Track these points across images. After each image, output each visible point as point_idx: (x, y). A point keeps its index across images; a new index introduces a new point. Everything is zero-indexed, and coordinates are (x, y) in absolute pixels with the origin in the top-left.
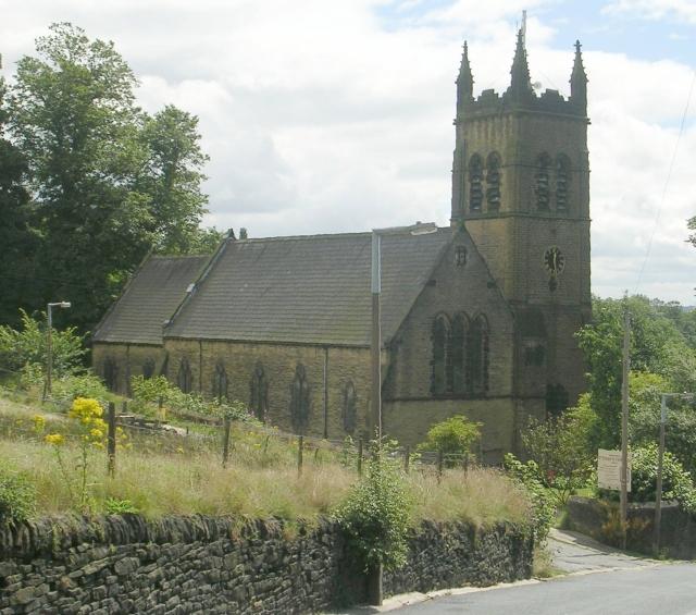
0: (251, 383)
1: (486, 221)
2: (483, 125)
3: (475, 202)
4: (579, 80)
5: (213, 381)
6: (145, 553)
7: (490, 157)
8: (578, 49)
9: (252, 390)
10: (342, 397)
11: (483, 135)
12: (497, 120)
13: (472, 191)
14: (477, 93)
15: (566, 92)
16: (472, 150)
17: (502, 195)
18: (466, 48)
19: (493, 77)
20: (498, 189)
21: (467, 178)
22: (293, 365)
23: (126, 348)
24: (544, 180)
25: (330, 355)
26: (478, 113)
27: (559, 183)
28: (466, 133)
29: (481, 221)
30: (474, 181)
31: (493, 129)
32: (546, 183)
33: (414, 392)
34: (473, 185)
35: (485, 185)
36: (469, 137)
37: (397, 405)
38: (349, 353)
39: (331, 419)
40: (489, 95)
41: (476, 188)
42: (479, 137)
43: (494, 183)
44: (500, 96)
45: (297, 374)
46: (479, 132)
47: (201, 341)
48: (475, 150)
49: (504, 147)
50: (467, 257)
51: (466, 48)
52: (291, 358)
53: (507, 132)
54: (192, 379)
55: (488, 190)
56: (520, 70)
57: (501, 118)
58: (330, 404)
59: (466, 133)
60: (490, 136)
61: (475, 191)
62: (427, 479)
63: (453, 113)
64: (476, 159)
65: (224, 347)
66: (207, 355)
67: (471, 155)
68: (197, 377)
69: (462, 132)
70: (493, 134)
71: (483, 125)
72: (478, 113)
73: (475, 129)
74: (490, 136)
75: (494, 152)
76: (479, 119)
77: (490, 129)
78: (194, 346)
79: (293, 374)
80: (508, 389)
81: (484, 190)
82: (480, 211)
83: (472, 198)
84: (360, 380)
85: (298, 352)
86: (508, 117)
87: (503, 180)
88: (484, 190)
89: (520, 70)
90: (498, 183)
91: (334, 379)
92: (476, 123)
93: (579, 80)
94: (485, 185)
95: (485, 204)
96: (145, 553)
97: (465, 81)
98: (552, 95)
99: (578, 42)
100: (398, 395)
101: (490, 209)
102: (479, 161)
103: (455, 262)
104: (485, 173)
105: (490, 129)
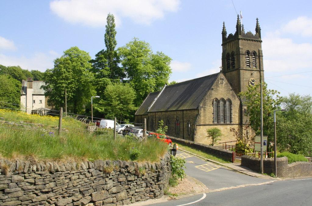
1: (231, 72)
2: (229, 45)
3: (228, 67)
4: (258, 30)
6: (172, 152)
7: (232, 53)
8: (257, 20)
10: (187, 125)
11: (229, 47)
12: (233, 42)
14: (227, 35)
15: (254, 33)
16: (227, 52)
17: (235, 63)
18: (224, 23)
19: (231, 30)
20: (234, 62)
21: (226, 60)
22: (175, 117)
24: (248, 58)
25: (184, 113)
26: (228, 41)
27: (253, 60)
28: (225, 47)
29: (230, 72)
30: (228, 61)
31: (232, 45)
32: (249, 60)
33: (207, 123)
34: (227, 62)
35: (231, 62)
37: (202, 127)
38: (188, 112)
39: (184, 132)
40: (231, 35)
41: (228, 63)
44: (234, 35)
46: (228, 46)
47: (155, 112)
48: (227, 52)
50: (224, 81)
51: (224, 23)
54: (154, 123)
56: (239, 27)
57: (234, 41)
58: (184, 127)
60: (231, 47)
61: (228, 64)
63: (221, 42)
65: (160, 113)
69: (224, 47)
72: (228, 41)
74: (231, 47)
75: (232, 52)
76: (228, 42)
77: (231, 45)
79: (175, 119)
80: (237, 122)
81: (231, 63)
82: (230, 69)
83: (227, 66)
84: (191, 119)
85: (176, 113)
86: (236, 40)
87: (236, 59)
88: (231, 63)
89: (239, 27)
92: (227, 44)
93: (258, 30)
94: (231, 62)
95: (231, 67)
96: (172, 152)
97: (224, 33)
98: (249, 34)
99: (257, 18)
100: (202, 124)
101: (232, 68)
102: (229, 55)
103: (220, 83)
104: (230, 58)
105: (231, 45)
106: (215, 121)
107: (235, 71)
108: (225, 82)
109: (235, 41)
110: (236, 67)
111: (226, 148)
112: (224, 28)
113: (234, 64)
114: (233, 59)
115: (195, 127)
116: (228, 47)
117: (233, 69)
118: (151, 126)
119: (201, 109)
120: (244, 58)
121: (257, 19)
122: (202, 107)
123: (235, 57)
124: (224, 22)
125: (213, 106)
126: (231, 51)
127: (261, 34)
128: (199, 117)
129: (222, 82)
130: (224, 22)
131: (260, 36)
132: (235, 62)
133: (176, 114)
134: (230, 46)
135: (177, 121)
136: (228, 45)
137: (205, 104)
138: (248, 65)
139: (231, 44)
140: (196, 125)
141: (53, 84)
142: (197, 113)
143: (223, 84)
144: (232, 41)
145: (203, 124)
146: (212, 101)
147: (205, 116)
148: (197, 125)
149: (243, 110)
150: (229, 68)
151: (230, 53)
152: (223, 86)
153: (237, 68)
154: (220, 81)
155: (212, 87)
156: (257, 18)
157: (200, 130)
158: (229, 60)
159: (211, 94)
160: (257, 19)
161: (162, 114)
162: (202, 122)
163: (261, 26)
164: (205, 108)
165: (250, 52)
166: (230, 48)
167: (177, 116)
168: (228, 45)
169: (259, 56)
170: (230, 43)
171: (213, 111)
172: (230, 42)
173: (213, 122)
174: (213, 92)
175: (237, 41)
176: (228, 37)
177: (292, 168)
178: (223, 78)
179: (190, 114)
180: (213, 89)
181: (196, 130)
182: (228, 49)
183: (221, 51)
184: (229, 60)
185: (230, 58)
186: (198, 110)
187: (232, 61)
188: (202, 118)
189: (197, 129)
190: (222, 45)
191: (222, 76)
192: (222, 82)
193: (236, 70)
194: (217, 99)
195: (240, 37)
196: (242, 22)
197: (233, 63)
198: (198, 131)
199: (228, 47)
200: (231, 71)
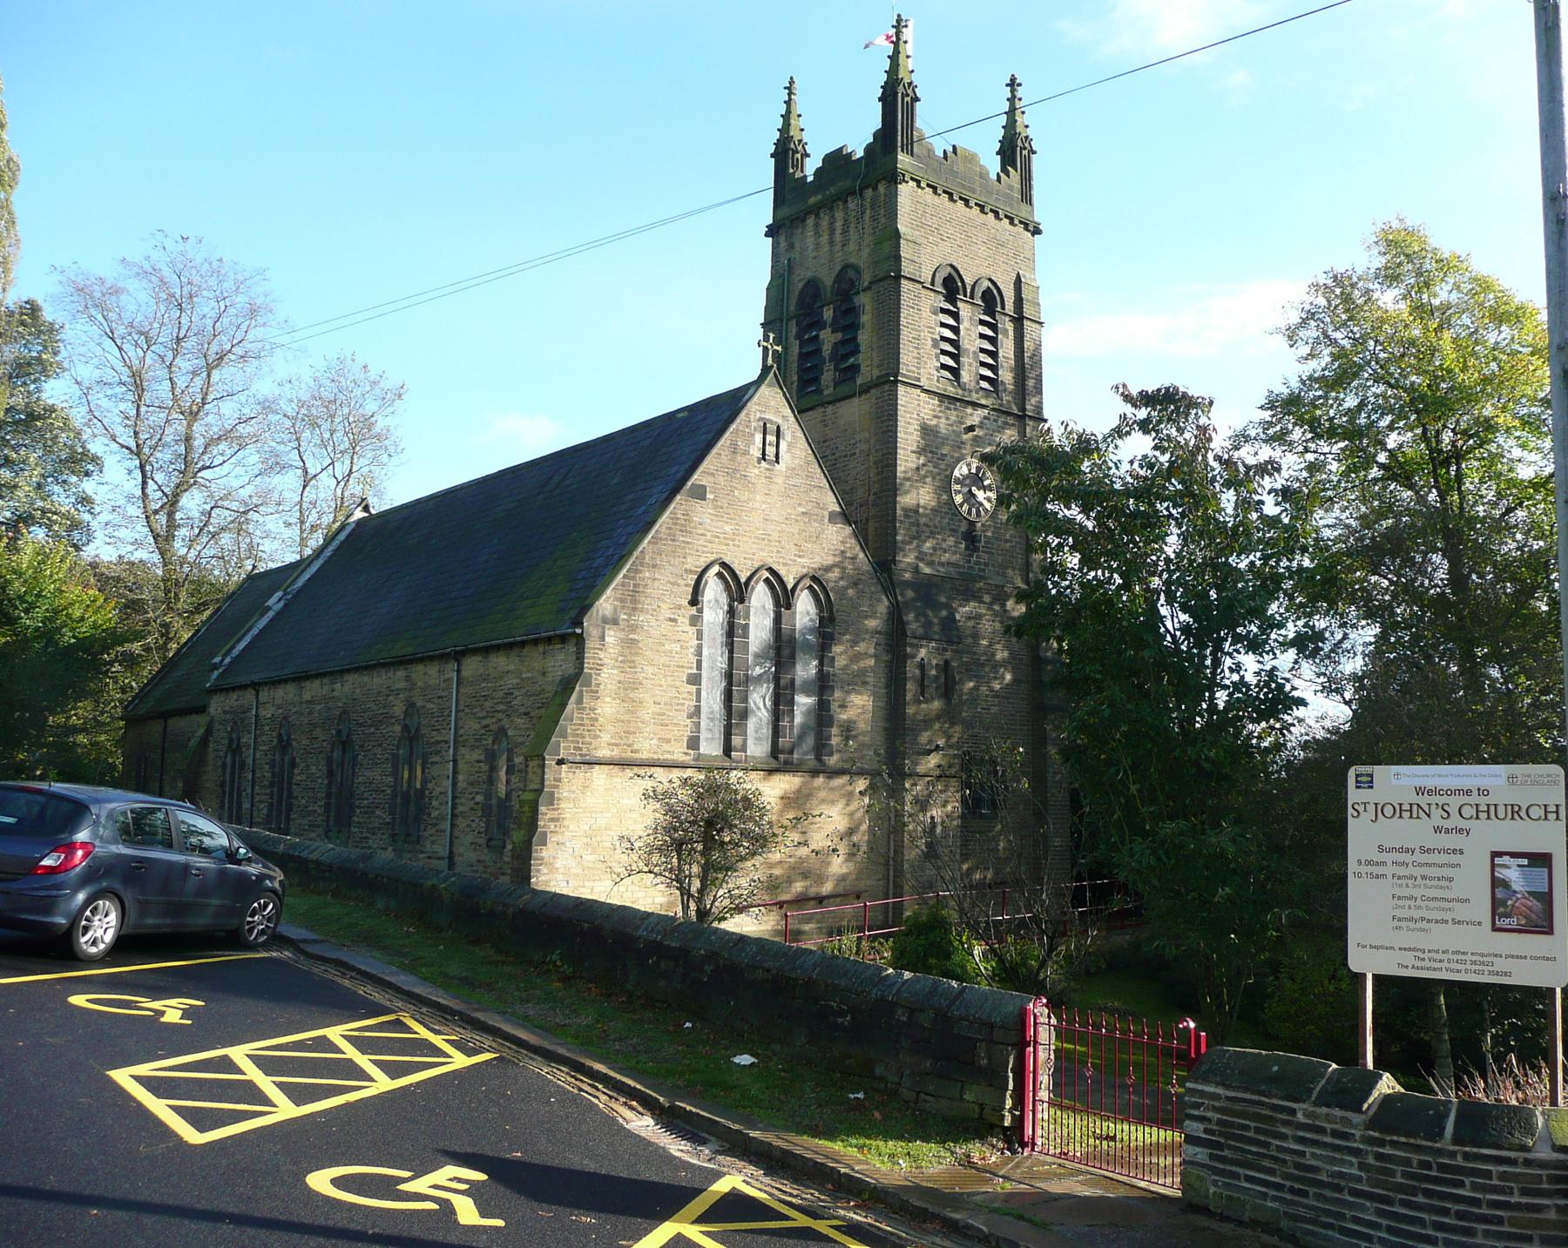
0: (330, 761)
1: (830, 409)
2: (825, 222)
4: (1013, 150)
5: (272, 764)
7: (839, 278)
9: (331, 774)
10: (485, 767)
11: (825, 239)
12: (852, 204)
13: (803, 357)
14: (811, 166)
17: (863, 348)
18: (790, 89)
20: (855, 338)
22: (399, 710)
23: (161, 722)
25: (465, 673)
28: (791, 246)
29: (821, 410)
32: (956, 330)
35: (828, 338)
36: (795, 254)
37: (599, 775)
40: (837, 161)
42: (817, 246)
43: (845, 329)
44: (860, 153)
45: (406, 728)
46: (817, 234)
48: (809, 274)
49: (866, 252)
51: (790, 89)
52: (397, 692)
53: (874, 219)
55: (835, 346)
58: (461, 785)
59: (791, 246)
60: (838, 237)
62: (213, 303)
63: (763, 211)
64: (813, 286)
66: (267, 713)
67: (801, 285)
68: (250, 761)
70: (845, 232)
71: (825, 222)
73: (810, 233)
74: (838, 237)
75: (846, 267)
76: (815, 210)
77: (839, 225)
78: (249, 696)
79: (398, 728)
81: (827, 349)
82: (819, 391)
86: (875, 188)
87: (865, 318)
88: (827, 349)
90: (854, 327)
91: (472, 726)
92: (810, 221)
93: (1013, 150)
95: (828, 376)
97: (786, 152)
100: (604, 753)
104: (828, 314)
105: (839, 225)
106: (703, 735)
107: (856, 400)
108: (795, 448)
109: (869, 193)
110: (868, 370)
111: (1004, 898)
112: (786, 117)
113: (856, 351)
114: (848, 322)
115: (549, 776)
116: (810, 241)
117: (845, 389)
118: (222, 785)
119: (602, 638)
120: (926, 313)
121: (1013, 84)
122: (615, 622)
123: (865, 300)
124: (792, 82)
125: (695, 620)
126: (838, 268)
127: (1035, 183)
128: (580, 701)
129: (771, 451)
130: (792, 82)
131: (1026, 196)
132: (863, 337)
133: (402, 685)
134: (832, 233)
135: (411, 739)
136: (817, 225)
137: (633, 600)
138: (944, 367)
139: (839, 215)
140: (550, 762)
141: (262, 932)
142: (570, 669)
143: (781, 467)
144: (843, 197)
145: (615, 753)
146: (693, 578)
147: (629, 687)
148: (560, 762)
149: (912, 670)
150: (816, 380)
151: (828, 281)
152: (780, 480)
153: (876, 373)
154: (758, 437)
155: (696, 478)
156: (1013, 79)
157: (591, 800)
158: (820, 324)
159: (685, 526)
160: (1013, 84)
161: (307, 696)
162: (605, 738)
163: (1034, 124)
164: (633, 628)
165: (969, 281)
166: (826, 248)
167: (410, 706)
168: (817, 225)
169: (1019, 320)
170: (831, 209)
171: (694, 660)
172: (828, 205)
173: (693, 743)
174: (702, 513)
175: (882, 188)
176: (818, 172)
177: (1544, 1178)
178: (779, 421)
179: (512, 681)
180: (700, 493)
181: (551, 800)
182: (810, 252)
183: (765, 277)
184: (820, 324)
185: (828, 314)
186: (580, 640)
187: (839, 335)
188: (607, 707)
189: (564, 792)
190: (771, 232)
191: (772, 404)
192: (771, 451)
193: (866, 389)
194: (727, 571)
195: (903, 160)
196: (920, 69)
197: (849, 346)
198: (567, 808)
199: (810, 241)
200: (822, 405)
